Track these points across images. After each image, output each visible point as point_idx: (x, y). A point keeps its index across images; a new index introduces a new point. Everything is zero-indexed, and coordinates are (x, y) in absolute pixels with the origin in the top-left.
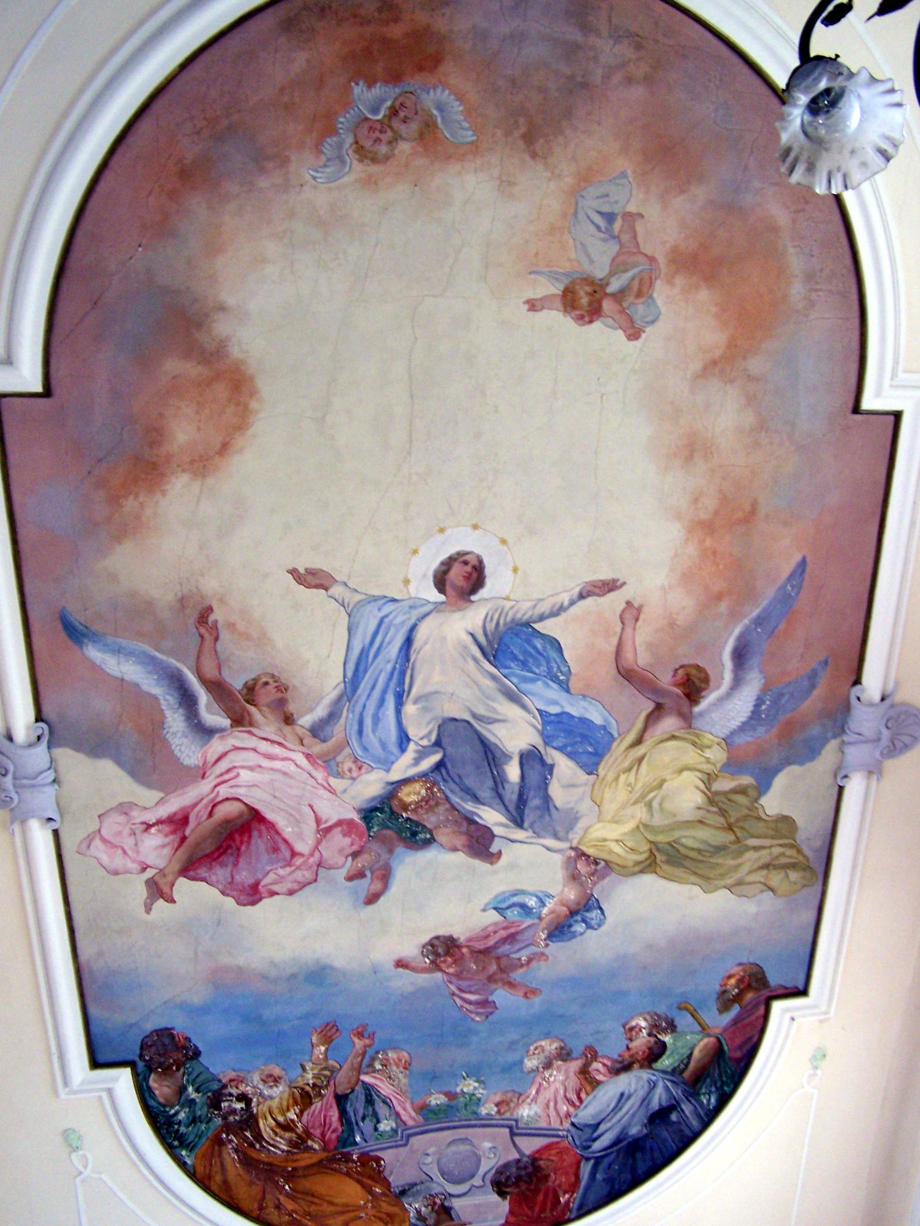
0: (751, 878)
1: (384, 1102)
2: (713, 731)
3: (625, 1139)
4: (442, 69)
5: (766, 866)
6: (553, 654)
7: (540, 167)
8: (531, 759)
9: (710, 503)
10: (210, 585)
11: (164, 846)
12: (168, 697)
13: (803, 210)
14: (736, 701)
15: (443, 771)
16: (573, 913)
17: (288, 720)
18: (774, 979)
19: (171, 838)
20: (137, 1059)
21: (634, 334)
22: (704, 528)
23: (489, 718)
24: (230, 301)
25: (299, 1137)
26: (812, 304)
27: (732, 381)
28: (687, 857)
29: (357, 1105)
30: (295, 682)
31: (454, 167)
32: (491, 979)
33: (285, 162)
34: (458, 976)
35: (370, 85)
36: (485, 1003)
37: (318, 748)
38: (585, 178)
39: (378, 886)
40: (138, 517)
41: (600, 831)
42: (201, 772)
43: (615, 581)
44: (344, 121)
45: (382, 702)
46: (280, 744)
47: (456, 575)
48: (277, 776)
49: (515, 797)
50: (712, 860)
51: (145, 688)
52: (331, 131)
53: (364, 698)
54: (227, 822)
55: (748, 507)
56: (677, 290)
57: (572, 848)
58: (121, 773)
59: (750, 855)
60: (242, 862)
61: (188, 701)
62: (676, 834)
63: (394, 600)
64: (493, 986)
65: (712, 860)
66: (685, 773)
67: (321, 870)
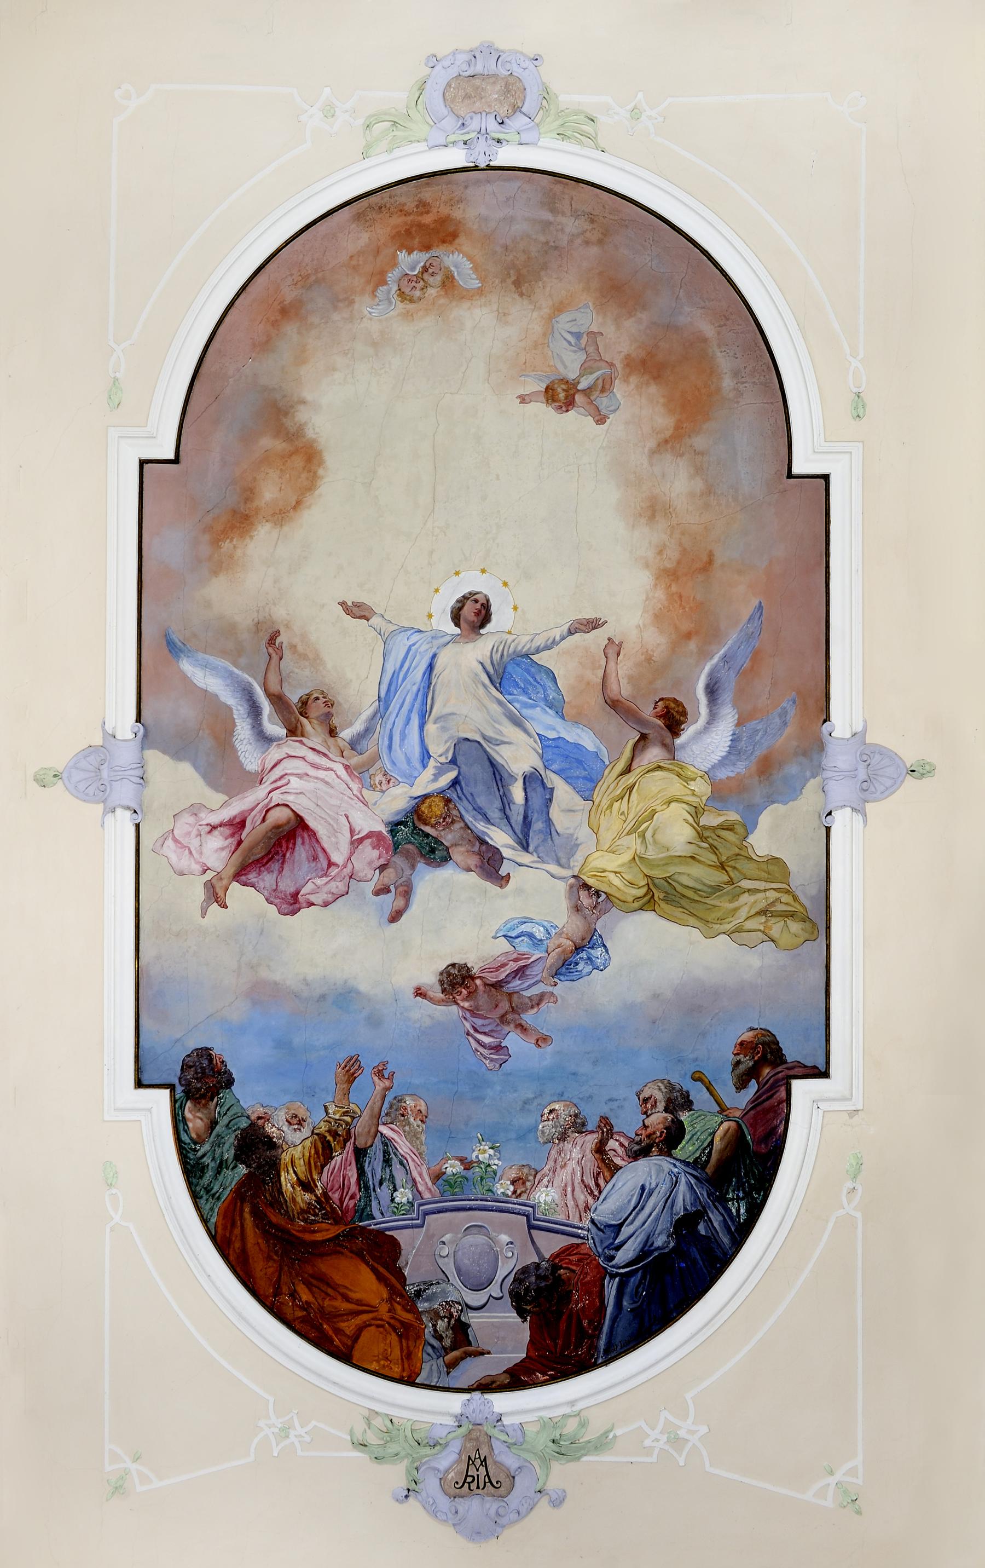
0: (749, 925)
1: (401, 1163)
2: (695, 763)
3: (651, 1252)
4: (457, 241)
5: (763, 912)
6: (549, 684)
7: (526, 302)
8: (532, 780)
9: (673, 554)
10: (280, 613)
11: (223, 849)
12: (239, 708)
13: (725, 325)
14: (713, 735)
15: (458, 788)
16: (578, 949)
17: (332, 732)
18: (791, 1053)
19: (230, 840)
20: (176, 1082)
21: (601, 420)
22: (669, 576)
23: (497, 740)
24: (308, 396)
25: (318, 1200)
26: (740, 394)
27: (682, 455)
28: (684, 896)
29: (374, 1165)
30: (340, 699)
31: (466, 304)
32: (503, 1019)
33: (352, 302)
34: (473, 1012)
35: (410, 252)
36: (498, 1048)
37: (355, 760)
38: (559, 309)
39: (400, 903)
40: (231, 557)
41: (601, 861)
42: (259, 778)
43: (597, 620)
44: (392, 276)
45: (408, 720)
46: (325, 755)
47: (469, 611)
48: (320, 785)
49: (521, 818)
50: (707, 901)
51: (223, 699)
52: (384, 282)
53: (394, 715)
54: (277, 827)
55: (705, 558)
56: (632, 386)
57: (574, 876)
58: (196, 775)
59: (745, 898)
60: (286, 871)
61: (255, 711)
62: (672, 870)
63: (420, 631)
64: (507, 1029)
65: (707, 901)
66: (673, 804)
67: (353, 882)
